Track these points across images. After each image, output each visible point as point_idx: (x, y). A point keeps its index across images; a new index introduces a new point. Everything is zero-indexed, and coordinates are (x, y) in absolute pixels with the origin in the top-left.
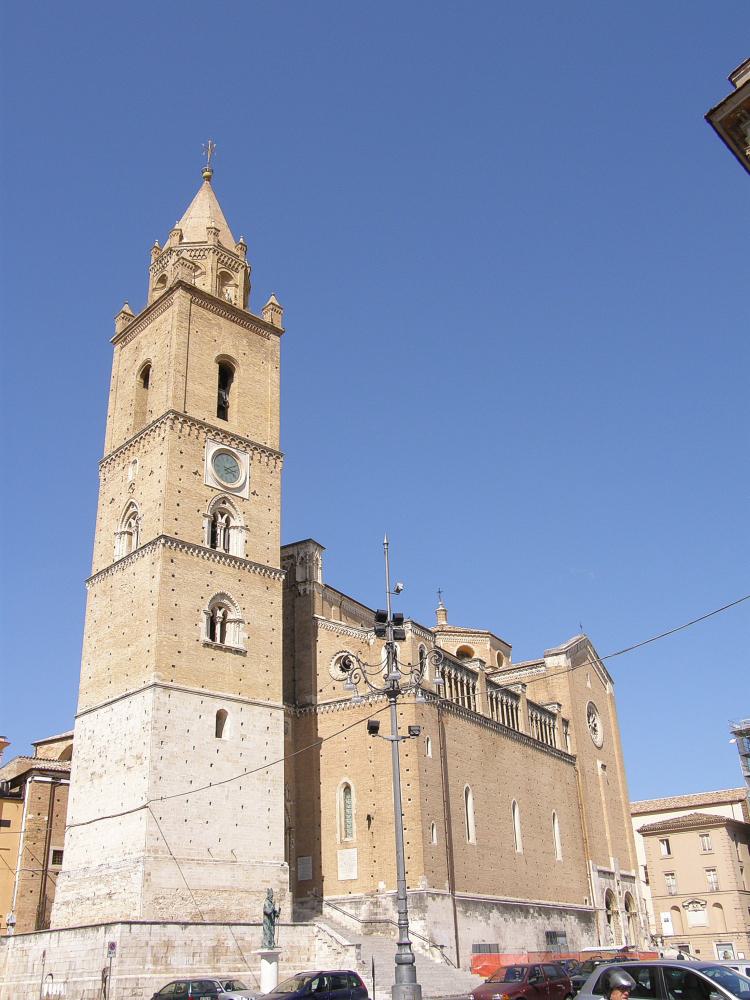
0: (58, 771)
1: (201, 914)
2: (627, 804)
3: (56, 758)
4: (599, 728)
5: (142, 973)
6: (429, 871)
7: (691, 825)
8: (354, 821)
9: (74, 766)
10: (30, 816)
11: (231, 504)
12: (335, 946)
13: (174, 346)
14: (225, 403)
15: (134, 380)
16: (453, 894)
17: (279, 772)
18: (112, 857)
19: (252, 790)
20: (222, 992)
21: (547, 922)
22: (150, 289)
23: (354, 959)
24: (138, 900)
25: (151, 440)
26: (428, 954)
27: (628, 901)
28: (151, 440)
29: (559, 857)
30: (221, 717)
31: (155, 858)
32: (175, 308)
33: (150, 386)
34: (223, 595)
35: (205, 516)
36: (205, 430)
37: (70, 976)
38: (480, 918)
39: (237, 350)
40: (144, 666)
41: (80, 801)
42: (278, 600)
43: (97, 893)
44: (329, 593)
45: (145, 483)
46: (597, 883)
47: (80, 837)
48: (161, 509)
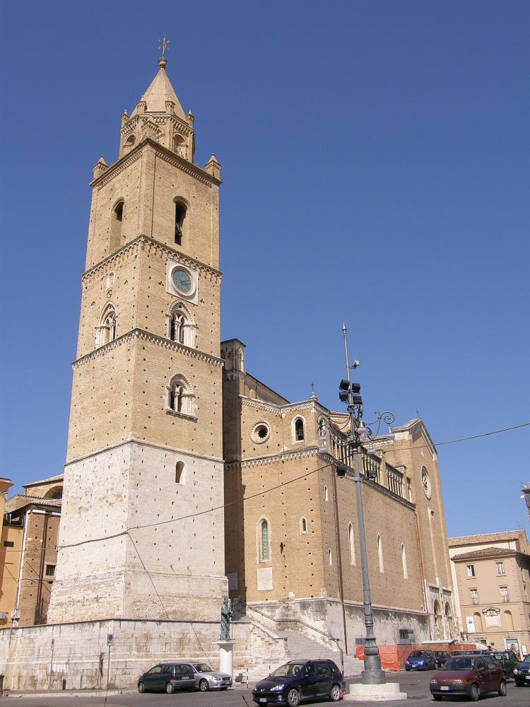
0: (50, 506)
1: (167, 613)
2: (446, 540)
4: (428, 485)
5: (129, 658)
6: (327, 585)
7: (487, 556)
8: (270, 547)
9: (64, 501)
10: (30, 539)
11: (185, 308)
12: (267, 638)
13: (144, 187)
14: (180, 232)
15: (110, 213)
16: (342, 601)
17: (221, 512)
18: (98, 571)
19: (202, 522)
20: (196, 672)
21: (399, 623)
22: (121, 146)
23: (283, 648)
24: (121, 603)
25: (126, 258)
26: (328, 645)
27: (447, 607)
28: (126, 258)
29: (406, 576)
30: (179, 467)
31: (133, 571)
32: (144, 159)
33: (123, 217)
34: (180, 376)
35: (167, 316)
36: (167, 251)
37: (71, 659)
38: (359, 619)
40: (122, 427)
41: (68, 528)
42: (219, 381)
43: (87, 597)
44: (249, 379)
45: (119, 289)
46: (429, 594)
47: (71, 555)
48: (135, 309)
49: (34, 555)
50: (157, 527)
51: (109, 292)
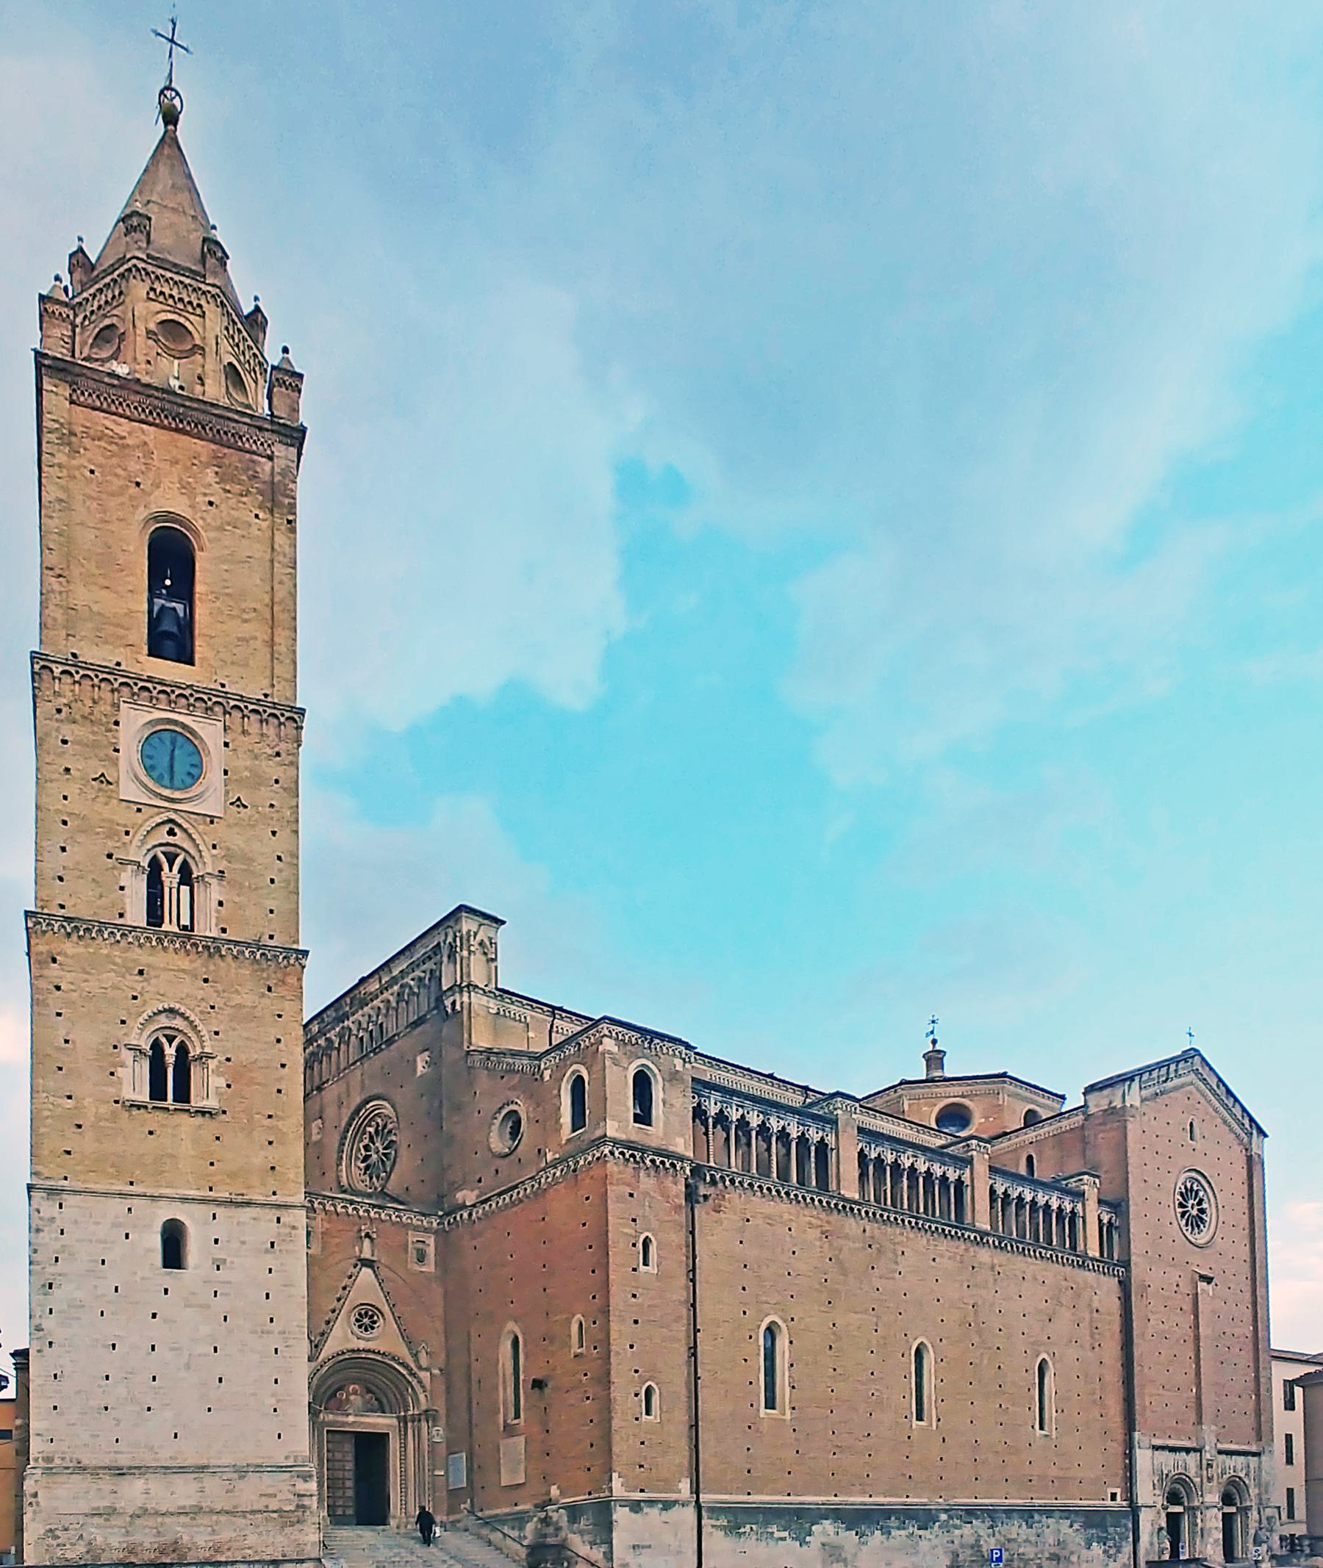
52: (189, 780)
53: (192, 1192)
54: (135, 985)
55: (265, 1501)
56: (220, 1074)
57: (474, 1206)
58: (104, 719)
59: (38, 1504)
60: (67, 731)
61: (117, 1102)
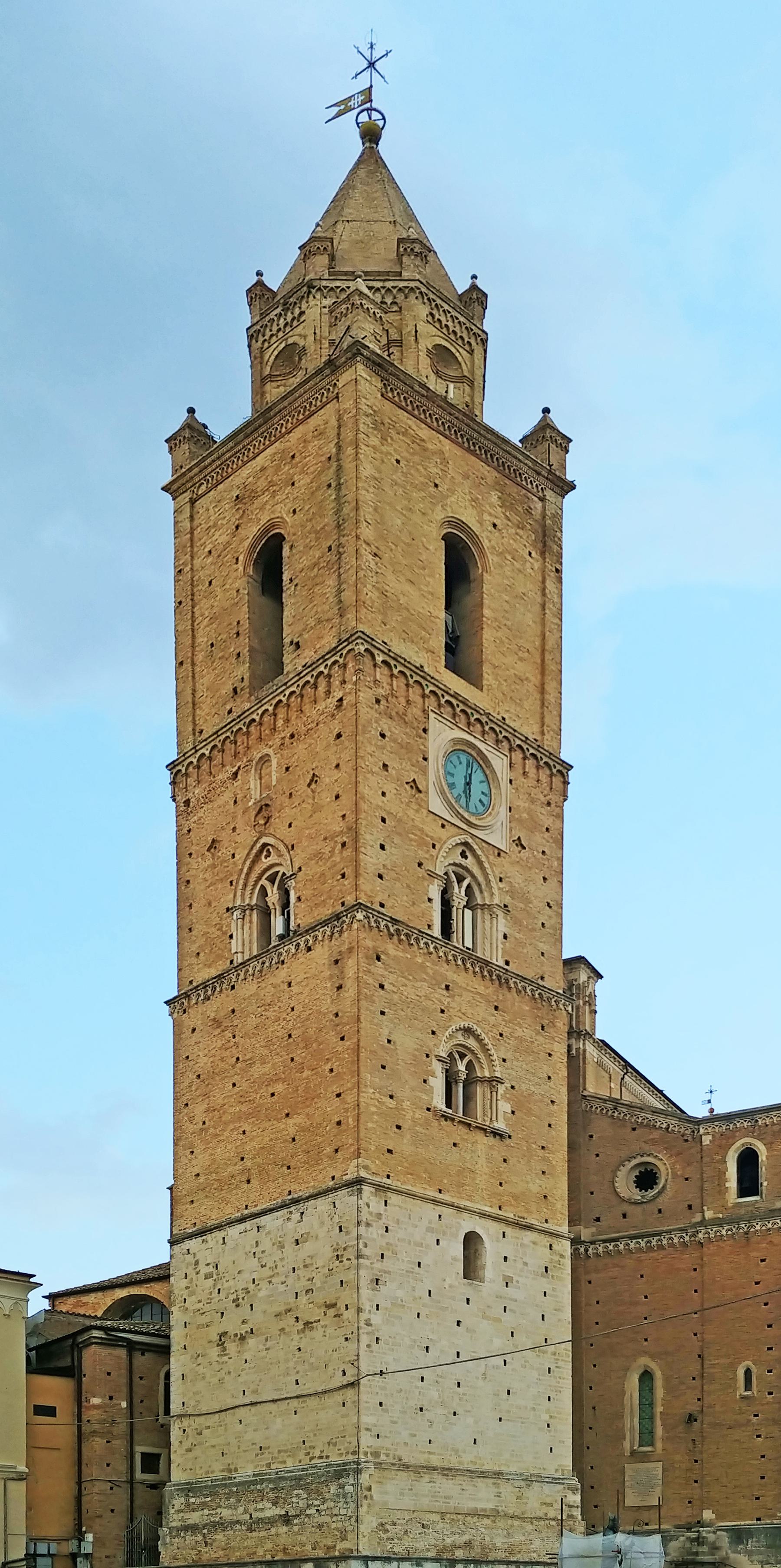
3: (99, 1314)
30: (471, 1241)
31: (376, 1464)
39: (481, 513)
40: (329, 1150)
49: (110, 1432)
50: (425, 1373)
51: (263, 808)
52: (481, 809)
53: (487, 1209)
54: (443, 999)
55: (545, 1509)
56: (508, 1100)
57: (592, 1243)
58: (416, 724)
59: (371, 1497)
60: (385, 725)
61: (428, 1109)
